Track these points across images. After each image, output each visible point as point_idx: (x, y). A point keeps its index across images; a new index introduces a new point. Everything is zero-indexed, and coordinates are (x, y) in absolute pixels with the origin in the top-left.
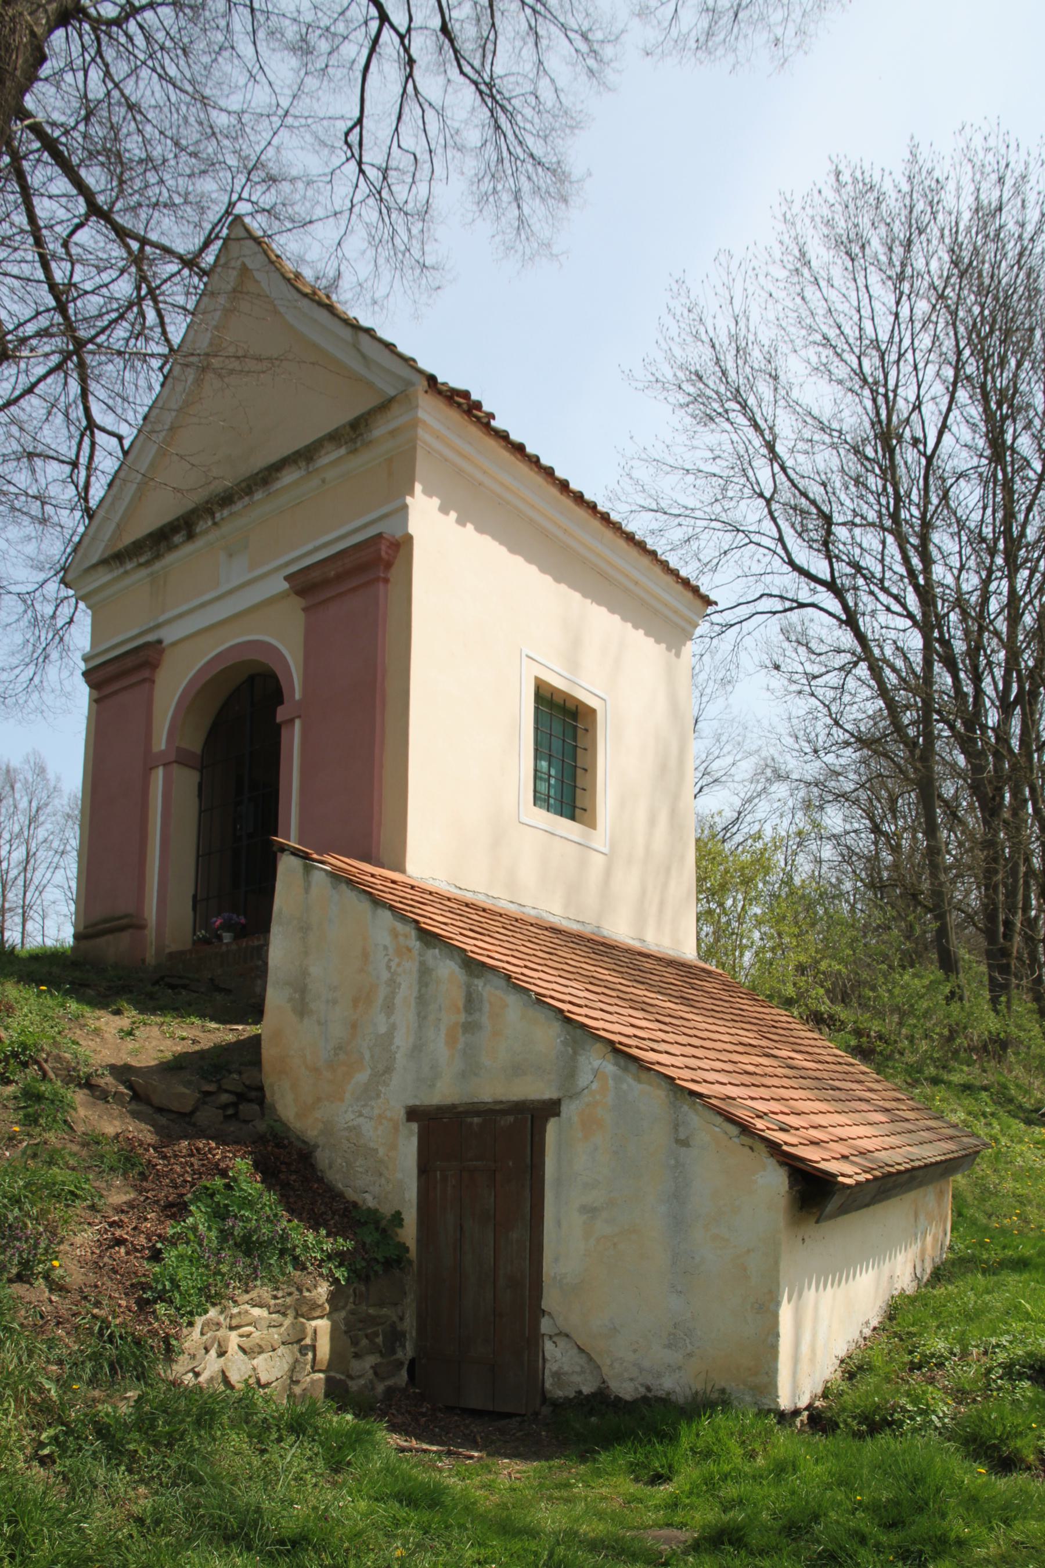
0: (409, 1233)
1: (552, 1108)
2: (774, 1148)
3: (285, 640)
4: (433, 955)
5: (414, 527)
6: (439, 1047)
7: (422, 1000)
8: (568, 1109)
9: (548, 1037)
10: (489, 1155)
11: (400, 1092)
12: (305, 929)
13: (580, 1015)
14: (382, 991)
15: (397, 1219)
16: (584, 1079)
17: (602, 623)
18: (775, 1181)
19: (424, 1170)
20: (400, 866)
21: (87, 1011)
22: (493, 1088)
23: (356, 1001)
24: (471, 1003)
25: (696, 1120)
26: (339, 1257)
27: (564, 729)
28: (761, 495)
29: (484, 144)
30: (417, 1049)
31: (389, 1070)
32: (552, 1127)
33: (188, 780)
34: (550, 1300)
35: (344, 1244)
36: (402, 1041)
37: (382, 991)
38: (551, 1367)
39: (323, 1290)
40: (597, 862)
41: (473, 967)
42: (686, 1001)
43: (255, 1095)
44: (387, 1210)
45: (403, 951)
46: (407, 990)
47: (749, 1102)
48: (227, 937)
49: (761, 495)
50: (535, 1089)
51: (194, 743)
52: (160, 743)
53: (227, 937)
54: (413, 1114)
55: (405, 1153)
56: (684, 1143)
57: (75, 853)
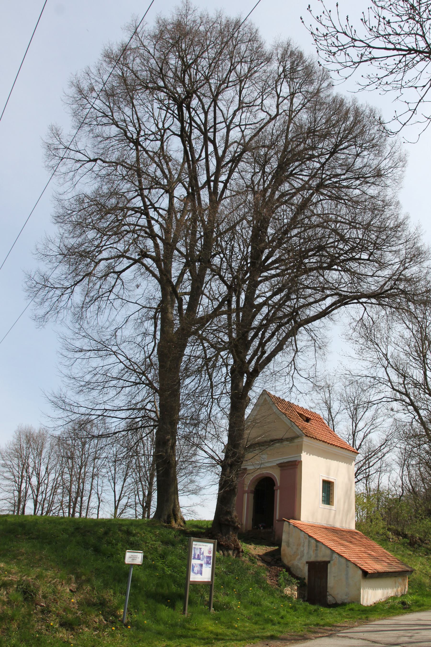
0: (306, 581)
1: (329, 562)
2: (360, 568)
3: (276, 475)
4: (310, 539)
5: (303, 459)
6: (311, 553)
7: (309, 545)
8: (331, 562)
9: (328, 552)
10: (319, 569)
11: (305, 559)
12: (289, 533)
13: (333, 548)
14: (302, 544)
15: (304, 579)
16: (334, 558)
17: (334, 464)
18: (360, 572)
19: (309, 571)
20: (299, 520)
21: (248, 545)
22: (320, 559)
23: (298, 545)
24: (317, 546)
25: (349, 564)
26: (298, 583)
27: (328, 487)
28: (384, 367)
30: (308, 553)
31: (303, 556)
32: (329, 565)
33: (252, 496)
34: (329, 590)
35: (299, 581)
36: (305, 552)
37: (302, 544)
38: (328, 600)
39: (296, 588)
40: (333, 512)
41: (317, 541)
42: (351, 542)
43: (280, 559)
44: (303, 577)
45: (306, 538)
46: (306, 544)
47: (359, 562)
48: (262, 528)
49: (384, 367)
50: (326, 559)
51: (253, 489)
52: (246, 489)
53: (262, 528)
54: (307, 562)
55: (306, 568)
56: (348, 567)
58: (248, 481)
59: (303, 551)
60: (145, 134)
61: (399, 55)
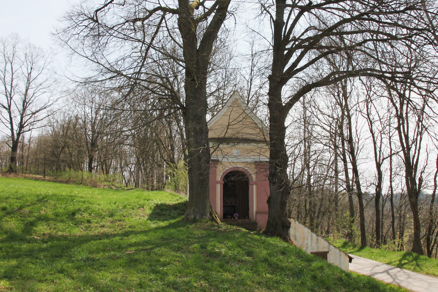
1: (328, 252)
6: (314, 245)
7: (312, 239)
8: (330, 252)
12: (295, 229)
22: (321, 250)
29: (425, 188)
30: (311, 245)
32: (328, 254)
36: (309, 244)
46: (310, 238)
50: (326, 250)
57: (287, 83)
58: (219, 173)
59: (308, 243)
60: (140, 52)
61: (273, 2)
